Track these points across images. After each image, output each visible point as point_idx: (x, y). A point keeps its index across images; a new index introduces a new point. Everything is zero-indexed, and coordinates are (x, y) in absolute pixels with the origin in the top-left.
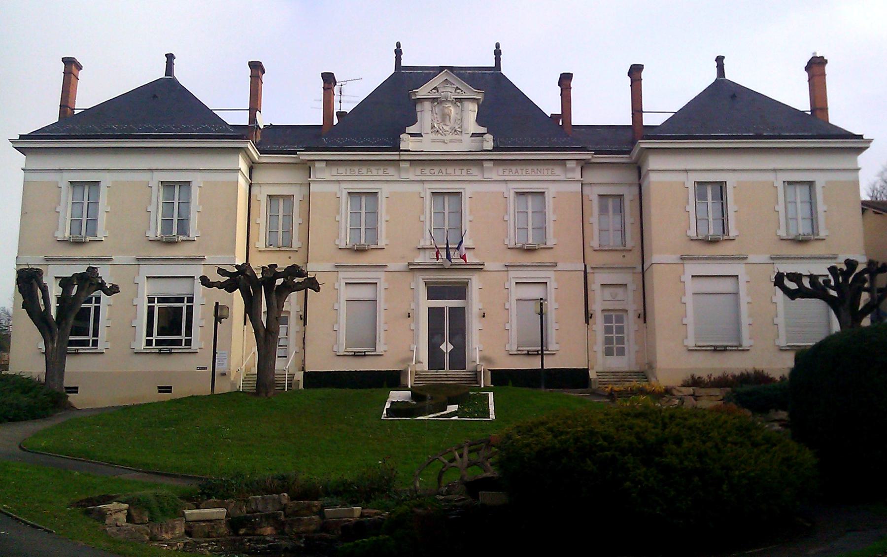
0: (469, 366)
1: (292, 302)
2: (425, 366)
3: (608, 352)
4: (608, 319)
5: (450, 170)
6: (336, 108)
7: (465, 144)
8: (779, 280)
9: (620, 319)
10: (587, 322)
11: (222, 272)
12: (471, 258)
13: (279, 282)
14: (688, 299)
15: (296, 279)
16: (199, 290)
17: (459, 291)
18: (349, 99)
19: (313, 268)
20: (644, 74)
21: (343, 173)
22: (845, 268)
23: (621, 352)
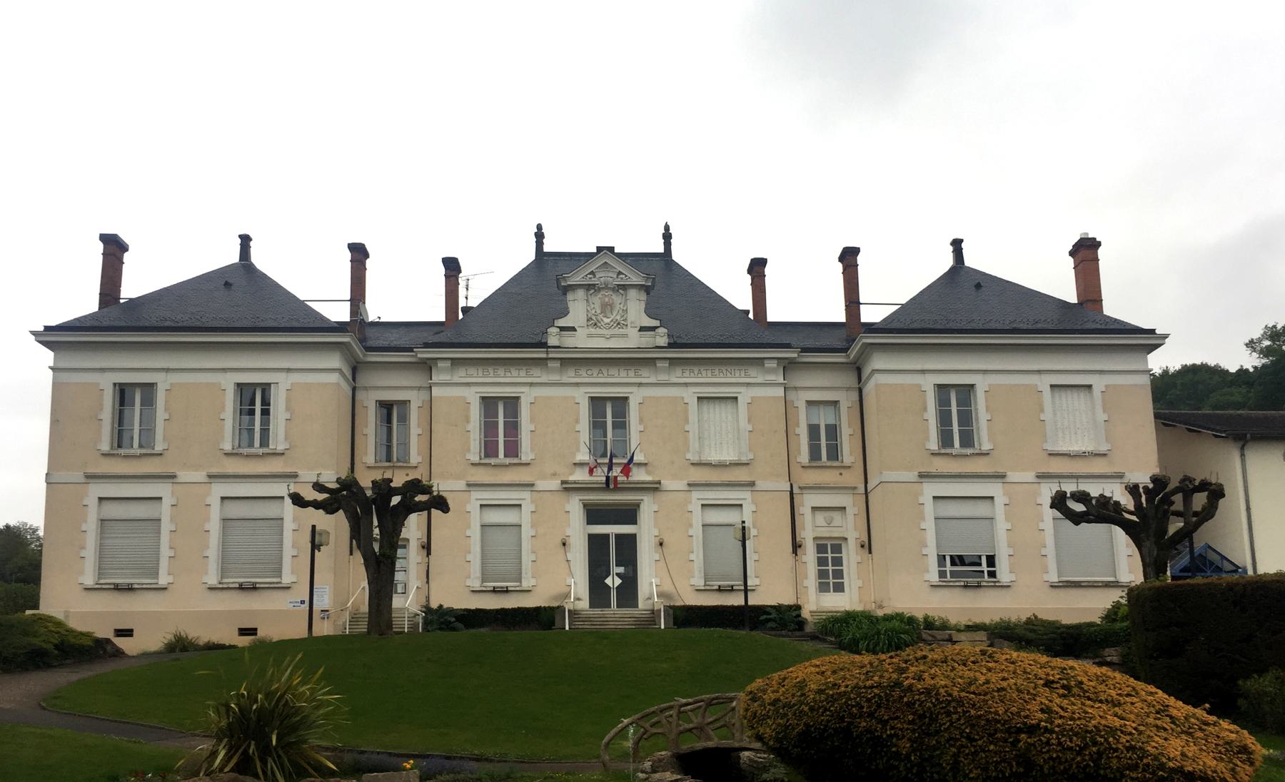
0: (642, 604)
1: (413, 527)
2: (584, 604)
3: (823, 588)
4: (821, 548)
5: (613, 371)
6: (462, 303)
7: (633, 340)
8: (1059, 502)
9: (837, 549)
10: (795, 552)
11: (318, 487)
12: (638, 475)
13: (396, 500)
14: (929, 525)
15: (423, 498)
16: (289, 507)
17: (629, 514)
18: (475, 293)
19: (441, 485)
20: (860, 259)
21: (475, 375)
22: (1151, 486)
23: (839, 588)
